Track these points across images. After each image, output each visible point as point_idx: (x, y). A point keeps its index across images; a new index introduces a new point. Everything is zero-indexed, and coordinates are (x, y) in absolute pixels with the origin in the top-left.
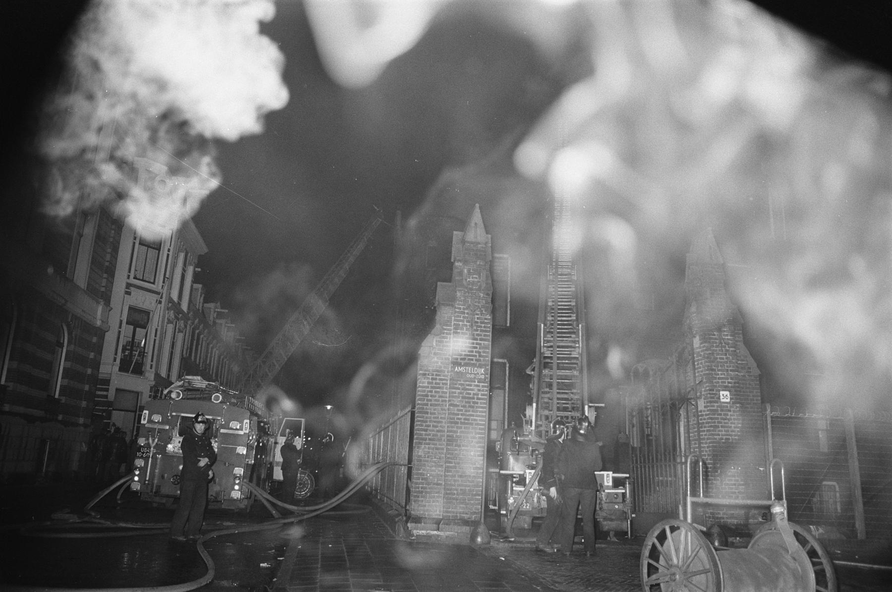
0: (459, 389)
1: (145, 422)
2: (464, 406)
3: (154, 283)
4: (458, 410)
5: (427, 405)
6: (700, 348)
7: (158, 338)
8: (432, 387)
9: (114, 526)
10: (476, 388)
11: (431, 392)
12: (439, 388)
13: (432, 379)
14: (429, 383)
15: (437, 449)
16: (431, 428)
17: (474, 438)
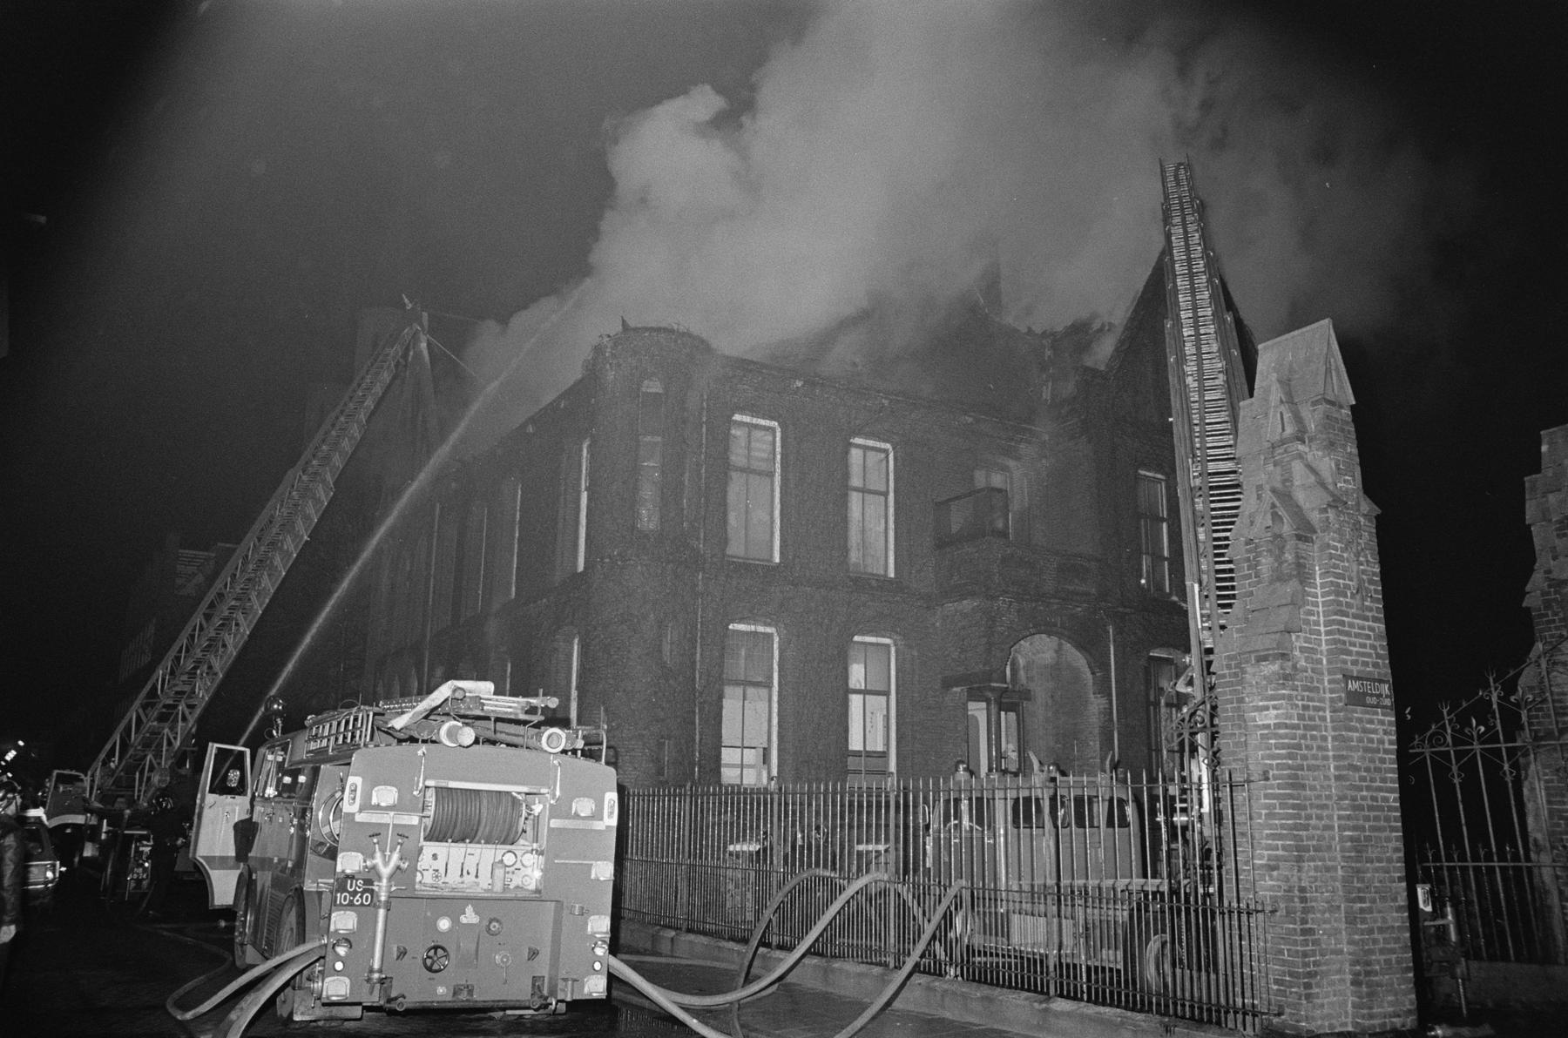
1: (355, 808)
2: (1367, 770)
4: (1363, 779)
8: (1306, 727)
11: (1304, 737)
12: (1314, 728)
13: (1305, 708)
15: (1328, 869)
16: (1313, 822)
17: (1388, 840)
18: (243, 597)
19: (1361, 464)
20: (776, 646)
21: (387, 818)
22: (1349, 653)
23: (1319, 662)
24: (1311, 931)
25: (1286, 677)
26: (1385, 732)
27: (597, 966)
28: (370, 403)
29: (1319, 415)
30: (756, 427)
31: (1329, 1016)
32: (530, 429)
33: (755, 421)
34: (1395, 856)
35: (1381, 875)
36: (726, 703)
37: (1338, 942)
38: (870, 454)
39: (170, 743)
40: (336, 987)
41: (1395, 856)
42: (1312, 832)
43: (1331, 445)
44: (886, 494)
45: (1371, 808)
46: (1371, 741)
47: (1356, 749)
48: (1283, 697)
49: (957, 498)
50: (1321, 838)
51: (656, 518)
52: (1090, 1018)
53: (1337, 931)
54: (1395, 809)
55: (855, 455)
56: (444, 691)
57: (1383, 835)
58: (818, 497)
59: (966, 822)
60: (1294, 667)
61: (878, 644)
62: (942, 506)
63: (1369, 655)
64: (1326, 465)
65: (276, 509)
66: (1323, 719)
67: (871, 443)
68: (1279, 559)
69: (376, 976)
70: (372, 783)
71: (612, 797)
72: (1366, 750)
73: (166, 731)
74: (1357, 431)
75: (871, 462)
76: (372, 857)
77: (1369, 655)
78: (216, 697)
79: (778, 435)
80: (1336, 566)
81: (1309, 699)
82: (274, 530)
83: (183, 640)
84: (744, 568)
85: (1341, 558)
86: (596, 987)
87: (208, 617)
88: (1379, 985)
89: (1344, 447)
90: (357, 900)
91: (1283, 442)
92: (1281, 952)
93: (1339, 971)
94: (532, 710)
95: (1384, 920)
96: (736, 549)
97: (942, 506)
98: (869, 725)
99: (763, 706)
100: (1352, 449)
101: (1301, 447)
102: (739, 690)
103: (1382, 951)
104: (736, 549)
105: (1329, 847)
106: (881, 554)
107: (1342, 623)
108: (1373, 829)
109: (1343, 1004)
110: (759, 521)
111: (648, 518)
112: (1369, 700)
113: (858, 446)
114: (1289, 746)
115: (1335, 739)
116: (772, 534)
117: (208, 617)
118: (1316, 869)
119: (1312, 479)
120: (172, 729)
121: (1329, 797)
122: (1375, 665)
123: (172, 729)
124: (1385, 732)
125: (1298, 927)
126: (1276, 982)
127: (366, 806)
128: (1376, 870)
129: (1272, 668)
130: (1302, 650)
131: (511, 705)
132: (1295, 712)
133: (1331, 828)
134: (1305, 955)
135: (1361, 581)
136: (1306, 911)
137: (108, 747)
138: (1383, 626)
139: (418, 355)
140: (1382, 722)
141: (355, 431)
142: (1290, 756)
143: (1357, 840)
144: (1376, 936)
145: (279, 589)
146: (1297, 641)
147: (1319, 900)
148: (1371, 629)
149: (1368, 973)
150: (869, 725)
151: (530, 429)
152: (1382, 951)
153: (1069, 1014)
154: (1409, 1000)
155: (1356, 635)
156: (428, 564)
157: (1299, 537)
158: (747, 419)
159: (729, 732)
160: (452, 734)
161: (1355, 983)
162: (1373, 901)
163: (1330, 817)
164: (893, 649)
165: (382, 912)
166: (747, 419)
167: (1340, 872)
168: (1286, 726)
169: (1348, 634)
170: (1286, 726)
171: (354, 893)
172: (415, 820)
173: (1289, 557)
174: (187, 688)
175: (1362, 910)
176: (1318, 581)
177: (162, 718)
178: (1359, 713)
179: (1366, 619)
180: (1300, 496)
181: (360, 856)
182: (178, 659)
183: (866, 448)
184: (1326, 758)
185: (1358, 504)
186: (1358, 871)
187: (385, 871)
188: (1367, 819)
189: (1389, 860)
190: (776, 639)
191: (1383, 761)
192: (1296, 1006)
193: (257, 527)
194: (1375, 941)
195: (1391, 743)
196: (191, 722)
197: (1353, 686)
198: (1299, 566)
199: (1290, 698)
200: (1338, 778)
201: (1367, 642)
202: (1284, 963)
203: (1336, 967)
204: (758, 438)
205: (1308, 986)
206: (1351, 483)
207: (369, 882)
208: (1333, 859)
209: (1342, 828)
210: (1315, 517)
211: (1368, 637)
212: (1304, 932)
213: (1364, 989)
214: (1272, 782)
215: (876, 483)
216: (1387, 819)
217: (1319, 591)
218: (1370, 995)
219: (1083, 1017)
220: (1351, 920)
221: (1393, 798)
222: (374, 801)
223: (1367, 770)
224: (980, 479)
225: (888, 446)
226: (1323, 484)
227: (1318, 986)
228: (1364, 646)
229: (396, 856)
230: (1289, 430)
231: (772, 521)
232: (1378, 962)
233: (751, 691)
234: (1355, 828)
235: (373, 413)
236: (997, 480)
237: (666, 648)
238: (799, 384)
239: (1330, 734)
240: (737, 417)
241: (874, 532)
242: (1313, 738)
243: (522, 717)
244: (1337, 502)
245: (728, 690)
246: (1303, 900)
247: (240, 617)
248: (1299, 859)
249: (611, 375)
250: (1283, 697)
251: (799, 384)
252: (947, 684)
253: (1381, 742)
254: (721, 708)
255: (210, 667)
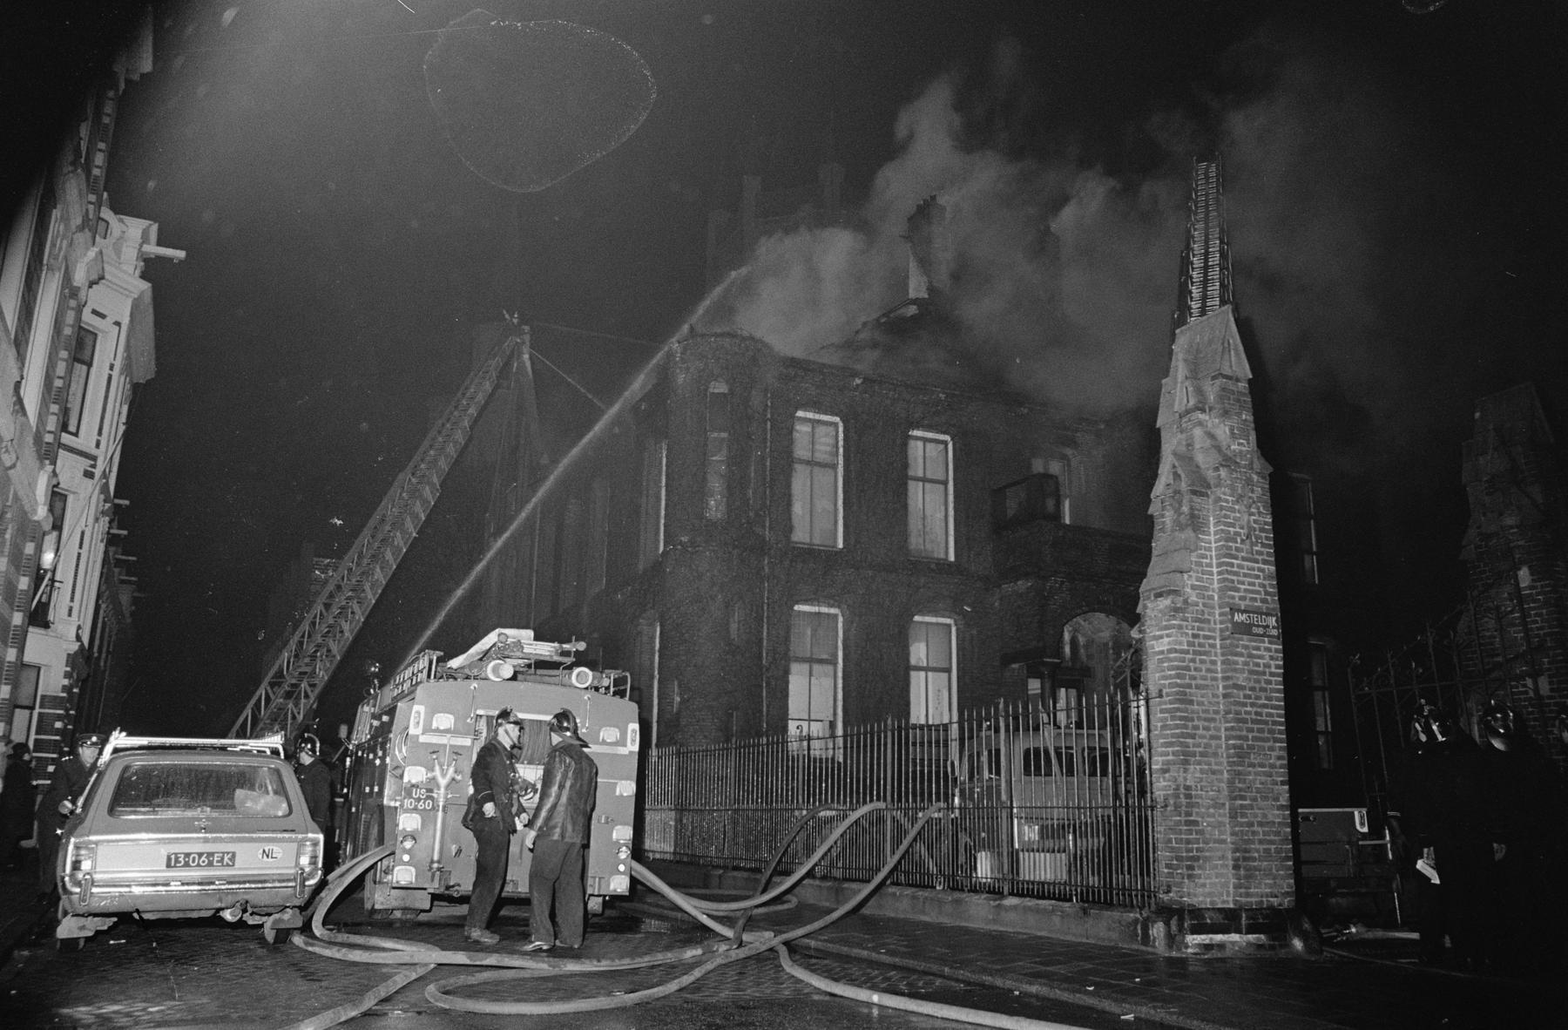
0: (1242, 655)
1: (419, 731)
2: (1253, 689)
3: (76, 435)
4: (1246, 696)
5: (1189, 686)
6: (1530, 588)
7: (84, 552)
8: (1195, 653)
9: (556, 971)
10: (1267, 654)
11: (1193, 661)
12: (1205, 653)
13: (1194, 636)
14: (1189, 644)
15: (1214, 772)
16: (1201, 732)
17: (1272, 749)
18: (357, 589)
19: (1257, 429)
20: (840, 625)
21: (443, 740)
22: (1238, 590)
23: (1211, 598)
24: (1195, 823)
25: (1176, 610)
26: (1272, 658)
27: (622, 868)
28: (472, 411)
29: (1216, 388)
30: (819, 421)
31: (1210, 894)
32: (617, 430)
33: (817, 417)
34: (1279, 763)
35: (1263, 778)
36: (792, 678)
37: (1221, 833)
38: (929, 446)
39: (294, 718)
40: (403, 874)
41: (1279, 763)
42: (1198, 740)
43: (1225, 414)
44: (945, 483)
45: (1253, 722)
46: (1258, 665)
47: (1242, 671)
48: (1173, 627)
49: (1014, 484)
50: (1207, 746)
51: (723, 508)
52: (1030, 909)
53: (1221, 824)
54: (1280, 724)
55: (802, 429)
56: (491, 639)
57: (1267, 745)
58: (877, 481)
59: (986, 775)
60: (1186, 602)
61: (938, 624)
62: (999, 493)
63: (1258, 592)
64: (1222, 431)
65: (389, 508)
66: (1213, 646)
67: (930, 435)
68: (1178, 512)
69: (435, 865)
70: (431, 713)
71: (634, 726)
72: (1251, 672)
73: (291, 706)
74: (1253, 401)
75: (930, 453)
76: (432, 770)
77: (1258, 592)
78: (333, 678)
79: (841, 429)
80: (1226, 516)
81: (1199, 629)
82: (388, 528)
83: (305, 626)
84: (809, 553)
85: (1234, 511)
86: (620, 885)
87: (327, 606)
88: (1256, 869)
89: (1239, 415)
90: (421, 806)
91: (1188, 412)
92: (1170, 841)
93: (1223, 857)
94: (565, 654)
95: (1265, 816)
96: (800, 535)
97: (999, 493)
98: (931, 699)
99: (828, 682)
100: (1247, 416)
101: (1202, 416)
102: (806, 666)
103: (1261, 842)
104: (800, 535)
105: (1215, 755)
106: (941, 538)
107: (1232, 565)
108: (1254, 739)
109: (1226, 885)
110: (818, 509)
111: (715, 507)
112: (1255, 630)
113: (917, 438)
114: (1178, 668)
115: (1223, 662)
116: (836, 522)
117: (327, 606)
118: (1202, 771)
119: (1208, 442)
120: (297, 705)
121: (1217, 712)
122: (1263, 601)
123: (297, 705)
124: (1272, 658)
125: (1183, 819)
126: (1167, 866)
127: (428, 729)
128: (1257, 774)
129: (1165, 602)
130: (1193, 587)
131: (546, 650)
132: (1184, 639)
133: (1219, 738)
134: (1188, 842)
135: (1251, 529)
136: (1190, 805)
137: (241, 719)
138: (1273, 568)
139: (522, 366)
140: (1269, 650)
141: (459, 437)
142: (1178, 676)
143: (1241, 747)
144: (1256, 828)
145: (391, 580)
146: (1189, 581)
147: (1204, 797)
148: (1260, 570)
149: (1245, 859)
150: (931, 699)
151: (617, 430)
152: (1261, 842)
153: (1015, 907)
154: (1288, 884)
155: (1245, 575)
156: (531, 555)
157: (1194, 492)
158: (810, 415)
159: (796, 705)
160: (496, 670)
161: (1236, 867)
162: (1255, 799)
163: (1218, 729)
164: (954, 629)
165: (440, 814)
166: (810, 415)
167: (1226, 775)
168: (1176, 651)
169: (1236, 574)
170: (1176, 651)
171: (419, 800)
172: (467, 742)
173: (1185, 509)
174: (308, 669)
175: (1242, 806)
176: (1212, 529)
177: (288, 695)
178: (1245, 640)
179: (1256, 561)
180: (1200, 458)
181: (423, 770)
182: (301, 643)
183: (925, 440)
184: (1215, 679)
185: (1252, 463)
186: (1239, 773)
187: (443, 782)
188: (1251, 730)
189: (1272, 766)
190: (841, 619)
191: (1269, 682)
192: (1180, 885)
193: (372, 523)
194: (1254, 833)
195: (1277, 667)
196: (312, 697)
197: (1239, 618)
198: (1193, 516)
199: (1180, 627)
200: (1225, 696)
201: (1256, 579)
202: (1173, 849)
203: (1219, 854)
204: (819, 434)
205: (1190, 868)
206: (1244, 446)
207: (430, 791)
208: (1219, 764)
209: (1228, 738)
210: (1210, 474)
211: (1258, 577)
212: (1188, 823)
213: (1242, 872)
214: (1166, 699)
215: (823, 450)
216: (1271, 732)
217: (1212, 538)
218: (1247, 877)
219: (1026, 909)
220: (1233, 815)
221: (1278, 715)
222: (434, 726)
223: (1253, 689)
224: (1038, 466)
225: (947, 438)
226: (1218, 448)
227: (1200, 868)
228: (1253, 584)
229: (451, 770)
230: (1192, 403)
231: (836, 510)
232: (1257, 851)
233: (816, 667)
234: (1239, 738)
235: (476, 421)
236: (1055, 468)
237: (734, 626)
238: (858, 381)
239: (1219, 659)
240: (800, 414)
241: (933, 518)
242: (1202, 662)
243: (557, 658)
244: (1228, 461)
245: (795, 668)
246: (1188, 796)
247: (356, 607)
248: (1186, 762)
249: (681, 378)
250: (1173, 627)
251: (858, 381)
252: (1007, 660)
253: (1267, 666)
254: (787, 683)
255: (329, 651)
